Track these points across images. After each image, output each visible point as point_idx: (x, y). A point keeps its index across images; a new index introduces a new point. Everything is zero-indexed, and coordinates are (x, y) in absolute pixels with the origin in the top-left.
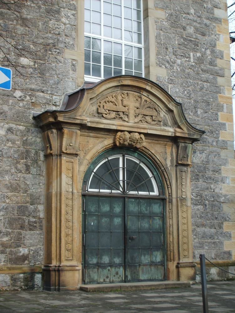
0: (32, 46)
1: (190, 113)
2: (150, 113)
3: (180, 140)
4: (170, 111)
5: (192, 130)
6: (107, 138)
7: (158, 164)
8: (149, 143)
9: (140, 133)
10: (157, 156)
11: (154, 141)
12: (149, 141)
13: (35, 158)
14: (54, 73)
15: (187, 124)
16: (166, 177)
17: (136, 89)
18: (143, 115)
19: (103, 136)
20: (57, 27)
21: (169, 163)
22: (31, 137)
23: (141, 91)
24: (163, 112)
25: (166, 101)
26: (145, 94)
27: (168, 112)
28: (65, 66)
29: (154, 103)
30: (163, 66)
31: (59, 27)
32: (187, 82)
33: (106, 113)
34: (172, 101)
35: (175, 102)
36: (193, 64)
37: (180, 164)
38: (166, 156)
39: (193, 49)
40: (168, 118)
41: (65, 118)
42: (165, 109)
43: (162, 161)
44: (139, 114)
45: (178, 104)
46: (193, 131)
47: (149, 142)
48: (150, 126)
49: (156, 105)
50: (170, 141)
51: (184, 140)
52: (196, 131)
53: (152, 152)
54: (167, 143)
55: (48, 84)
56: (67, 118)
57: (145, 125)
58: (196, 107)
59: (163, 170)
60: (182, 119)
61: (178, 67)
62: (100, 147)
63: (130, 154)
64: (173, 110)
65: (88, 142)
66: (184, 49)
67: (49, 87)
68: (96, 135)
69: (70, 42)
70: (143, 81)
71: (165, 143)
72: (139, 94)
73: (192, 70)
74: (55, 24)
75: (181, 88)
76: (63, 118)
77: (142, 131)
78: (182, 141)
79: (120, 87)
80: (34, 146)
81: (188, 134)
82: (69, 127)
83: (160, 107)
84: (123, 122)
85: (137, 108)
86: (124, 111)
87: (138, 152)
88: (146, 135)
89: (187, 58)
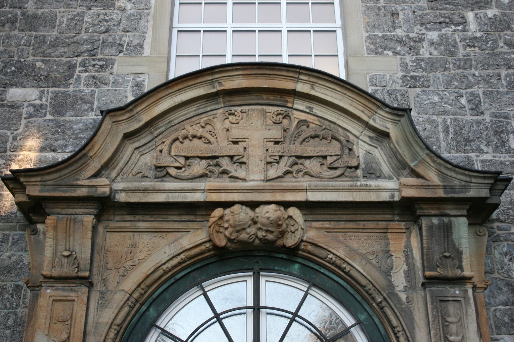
0: (39, 64)
1: (483, 147)
2: (318, 149)
3: (422, 209)
4: (384, 135)
5: (454, 175)
6: (192, 231)
7: (365, 287)
8: (328, 230)
9: (286, 205)
10: (357, 267)
11: (342, 224)
12: (326, 225)
13: (11, 304)
14: (85, 107)
15: (434, 162)
16: (395, 322)
17: (272, 98)
18: (294, 158)
19: (176, 225)
20: (103, 19)
21: (399, 281)
22: (8, 254)
23: (287, 102)
24: (363, 143)
25: (363, 112)
26: (300, 104)
27: (378, 140)
28: (116, 90)
29: (333, 125)
30: (386, 52)
31: (107, 18)
32: (464, 76)
33: (178, 165)
34: (378, 107)
35: (387, 109)
36: (478, 35)
37: (441, 280)
38: (389, 261)
39: (472, 4)
40: (380, 155)
41: (47, 188)
42: (365, 134)
43: (379, 279)
44: (281, 157)
45: (397, 112)
46: (459, 177)
47: (327, 228)
48: (314, 183)
49: (340, 129)
50: (397, 218)
51: (438, 209)
52: (470, 176)
53: (338, 254)
54: (387, 225)
55: (69, 132)
56: (51, 187)
57: (305, 182)
58: (502, 132)
59: (380, 302)
60: (418, 149)
61: (432, 50)
62: (167, 254)
63: (276, 268)
64: (388, 131)
65: (134, 245)
66: (445, 9)
67: (70, 138)
68: (156, 225)
69: (132, 41)
70: (284, 73)
71: (382, 224)
72: (280, 109)
73: (477, 49)
74: (99, 15)
75: (446, 93)
76: (39, 188)
77: (290, 197)
78: (433, 212)
79: (221, 100)
80: (13, 275)
81: (445, 187)
82: (64, 211)
83: (351, 133)
84: (231, 182)
85: (277, 143)
86: (232, 154)
87: (299, 260)
88: (306, 206)
89: (458, 24)
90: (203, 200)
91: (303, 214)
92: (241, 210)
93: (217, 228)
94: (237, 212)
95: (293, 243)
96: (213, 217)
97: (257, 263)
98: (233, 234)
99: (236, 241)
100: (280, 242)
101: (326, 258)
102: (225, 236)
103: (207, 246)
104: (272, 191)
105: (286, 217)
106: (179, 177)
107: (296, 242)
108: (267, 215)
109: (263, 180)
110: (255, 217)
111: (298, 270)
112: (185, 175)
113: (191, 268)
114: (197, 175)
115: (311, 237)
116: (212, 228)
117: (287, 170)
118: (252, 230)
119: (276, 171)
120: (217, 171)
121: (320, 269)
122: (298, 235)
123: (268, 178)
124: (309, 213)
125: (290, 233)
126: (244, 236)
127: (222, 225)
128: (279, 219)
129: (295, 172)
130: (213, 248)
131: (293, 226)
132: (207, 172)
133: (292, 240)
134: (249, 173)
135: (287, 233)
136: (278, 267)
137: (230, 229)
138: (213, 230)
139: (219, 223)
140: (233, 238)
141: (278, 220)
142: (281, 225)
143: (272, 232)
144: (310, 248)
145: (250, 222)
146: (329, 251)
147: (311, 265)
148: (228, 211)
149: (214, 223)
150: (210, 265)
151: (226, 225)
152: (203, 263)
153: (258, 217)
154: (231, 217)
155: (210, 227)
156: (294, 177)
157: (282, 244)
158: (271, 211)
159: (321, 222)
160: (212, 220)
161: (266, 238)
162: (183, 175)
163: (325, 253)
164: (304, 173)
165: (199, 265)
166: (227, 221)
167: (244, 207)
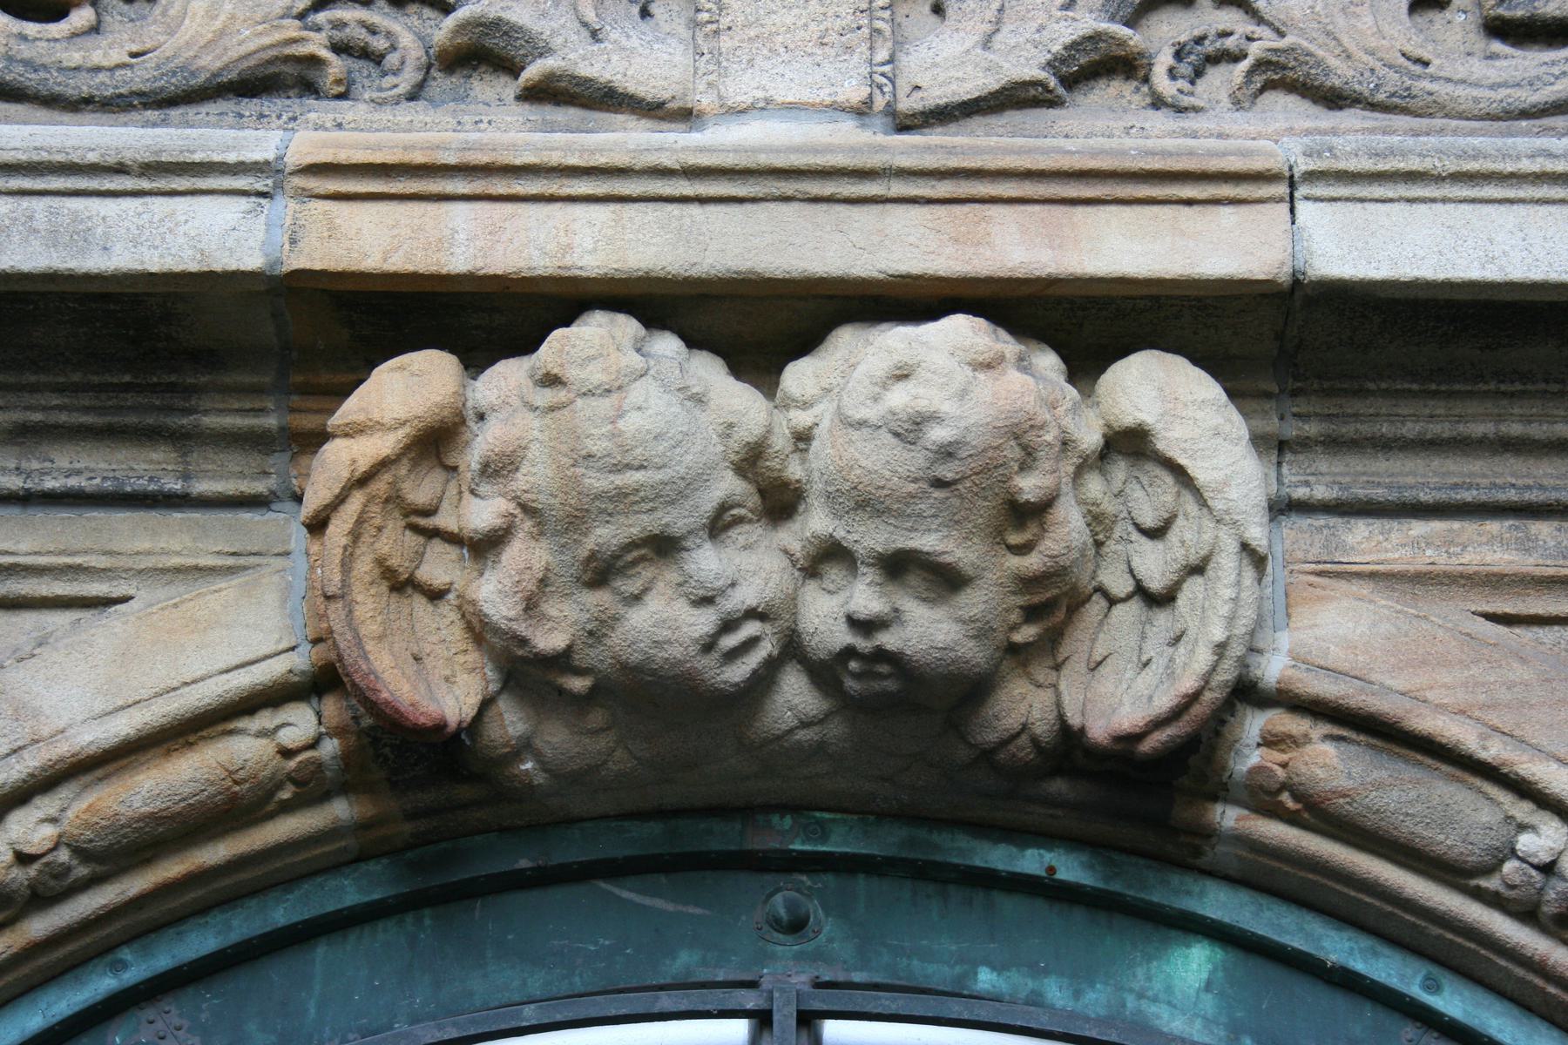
6: (144, 594)
9: (1082, 324)
12: (1488, 547)
47: (1495, 581)
63: (986, 979)
90: (252, 261)
91: (1262, 443)
92: (636, 361)
93: (394, 543)
94: (595, 375)
95: (1164, 702)
96: (354, 431)
97: (796, 926)
98: (552, 608)
99: (578, 684)
100: (1023, 706)
101: (1492, 869)
102: (479, 630)
103: (289, 737)
104: (944, 189)
105: (1090, 438)
106: (31, 79)
107: (1188, 684)
108: (900, 398)
109: (861, 111)
110: (781, 441)
111: (1209, 1003)
112: (97, 58)
113: (118, 967)
114: (210, 63)
115: (1337, 656)
116: (338, 529)
117: (1095, 38)
118: (753, 567)
119: (987, 43)
120: (406, 39)
121: (1433, 986)
122: (1212, 614)
123: (906, 104)
124: (1312, 429)
125: (1131, 611)
126: (661, 621)
127: (445, 520)
128: (1023, 441)
129: (1164, 60)
130: (346, 757)
131: (1156, 533)
132: (316, 45)
133: (1149, 677)
134: (726, 42)
135: (1097, 605)
136: (998, 967)
137: (525, 555)
138: (347, 565)
139: (421, 491)
140: (550, 640)
141: (1013, 452)
142: (1027, 515)
143: (946, 580)
144: (1327, 762)
145: (728, 485)
146: (1523, 789)
147: (1339, 947)
148: (507, 378)
149: (363, 481)
150: (321, 952)
151: (482, 514)
152: (241, 925)
153: (803, 438)
154: (530, 427)
155: (317, 526)
156: (1158, 103)
157: (1043, 727)
158: (940, 360)
159: (1437, 526)
160: (339, 459)
161: (889, 640)
162: (75, 57)
163: (1487, 815)
164: (1261, 65)
165: (200, 942)
166: (497, 469)
167: (668, 345)
